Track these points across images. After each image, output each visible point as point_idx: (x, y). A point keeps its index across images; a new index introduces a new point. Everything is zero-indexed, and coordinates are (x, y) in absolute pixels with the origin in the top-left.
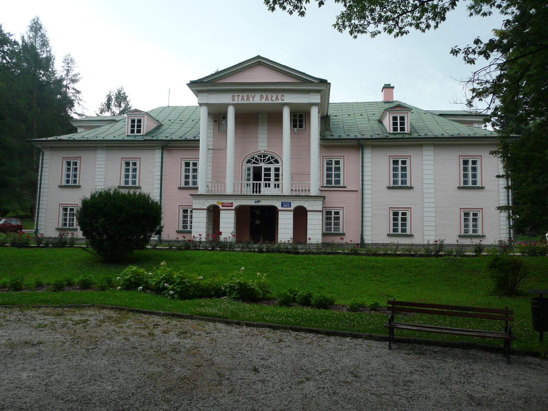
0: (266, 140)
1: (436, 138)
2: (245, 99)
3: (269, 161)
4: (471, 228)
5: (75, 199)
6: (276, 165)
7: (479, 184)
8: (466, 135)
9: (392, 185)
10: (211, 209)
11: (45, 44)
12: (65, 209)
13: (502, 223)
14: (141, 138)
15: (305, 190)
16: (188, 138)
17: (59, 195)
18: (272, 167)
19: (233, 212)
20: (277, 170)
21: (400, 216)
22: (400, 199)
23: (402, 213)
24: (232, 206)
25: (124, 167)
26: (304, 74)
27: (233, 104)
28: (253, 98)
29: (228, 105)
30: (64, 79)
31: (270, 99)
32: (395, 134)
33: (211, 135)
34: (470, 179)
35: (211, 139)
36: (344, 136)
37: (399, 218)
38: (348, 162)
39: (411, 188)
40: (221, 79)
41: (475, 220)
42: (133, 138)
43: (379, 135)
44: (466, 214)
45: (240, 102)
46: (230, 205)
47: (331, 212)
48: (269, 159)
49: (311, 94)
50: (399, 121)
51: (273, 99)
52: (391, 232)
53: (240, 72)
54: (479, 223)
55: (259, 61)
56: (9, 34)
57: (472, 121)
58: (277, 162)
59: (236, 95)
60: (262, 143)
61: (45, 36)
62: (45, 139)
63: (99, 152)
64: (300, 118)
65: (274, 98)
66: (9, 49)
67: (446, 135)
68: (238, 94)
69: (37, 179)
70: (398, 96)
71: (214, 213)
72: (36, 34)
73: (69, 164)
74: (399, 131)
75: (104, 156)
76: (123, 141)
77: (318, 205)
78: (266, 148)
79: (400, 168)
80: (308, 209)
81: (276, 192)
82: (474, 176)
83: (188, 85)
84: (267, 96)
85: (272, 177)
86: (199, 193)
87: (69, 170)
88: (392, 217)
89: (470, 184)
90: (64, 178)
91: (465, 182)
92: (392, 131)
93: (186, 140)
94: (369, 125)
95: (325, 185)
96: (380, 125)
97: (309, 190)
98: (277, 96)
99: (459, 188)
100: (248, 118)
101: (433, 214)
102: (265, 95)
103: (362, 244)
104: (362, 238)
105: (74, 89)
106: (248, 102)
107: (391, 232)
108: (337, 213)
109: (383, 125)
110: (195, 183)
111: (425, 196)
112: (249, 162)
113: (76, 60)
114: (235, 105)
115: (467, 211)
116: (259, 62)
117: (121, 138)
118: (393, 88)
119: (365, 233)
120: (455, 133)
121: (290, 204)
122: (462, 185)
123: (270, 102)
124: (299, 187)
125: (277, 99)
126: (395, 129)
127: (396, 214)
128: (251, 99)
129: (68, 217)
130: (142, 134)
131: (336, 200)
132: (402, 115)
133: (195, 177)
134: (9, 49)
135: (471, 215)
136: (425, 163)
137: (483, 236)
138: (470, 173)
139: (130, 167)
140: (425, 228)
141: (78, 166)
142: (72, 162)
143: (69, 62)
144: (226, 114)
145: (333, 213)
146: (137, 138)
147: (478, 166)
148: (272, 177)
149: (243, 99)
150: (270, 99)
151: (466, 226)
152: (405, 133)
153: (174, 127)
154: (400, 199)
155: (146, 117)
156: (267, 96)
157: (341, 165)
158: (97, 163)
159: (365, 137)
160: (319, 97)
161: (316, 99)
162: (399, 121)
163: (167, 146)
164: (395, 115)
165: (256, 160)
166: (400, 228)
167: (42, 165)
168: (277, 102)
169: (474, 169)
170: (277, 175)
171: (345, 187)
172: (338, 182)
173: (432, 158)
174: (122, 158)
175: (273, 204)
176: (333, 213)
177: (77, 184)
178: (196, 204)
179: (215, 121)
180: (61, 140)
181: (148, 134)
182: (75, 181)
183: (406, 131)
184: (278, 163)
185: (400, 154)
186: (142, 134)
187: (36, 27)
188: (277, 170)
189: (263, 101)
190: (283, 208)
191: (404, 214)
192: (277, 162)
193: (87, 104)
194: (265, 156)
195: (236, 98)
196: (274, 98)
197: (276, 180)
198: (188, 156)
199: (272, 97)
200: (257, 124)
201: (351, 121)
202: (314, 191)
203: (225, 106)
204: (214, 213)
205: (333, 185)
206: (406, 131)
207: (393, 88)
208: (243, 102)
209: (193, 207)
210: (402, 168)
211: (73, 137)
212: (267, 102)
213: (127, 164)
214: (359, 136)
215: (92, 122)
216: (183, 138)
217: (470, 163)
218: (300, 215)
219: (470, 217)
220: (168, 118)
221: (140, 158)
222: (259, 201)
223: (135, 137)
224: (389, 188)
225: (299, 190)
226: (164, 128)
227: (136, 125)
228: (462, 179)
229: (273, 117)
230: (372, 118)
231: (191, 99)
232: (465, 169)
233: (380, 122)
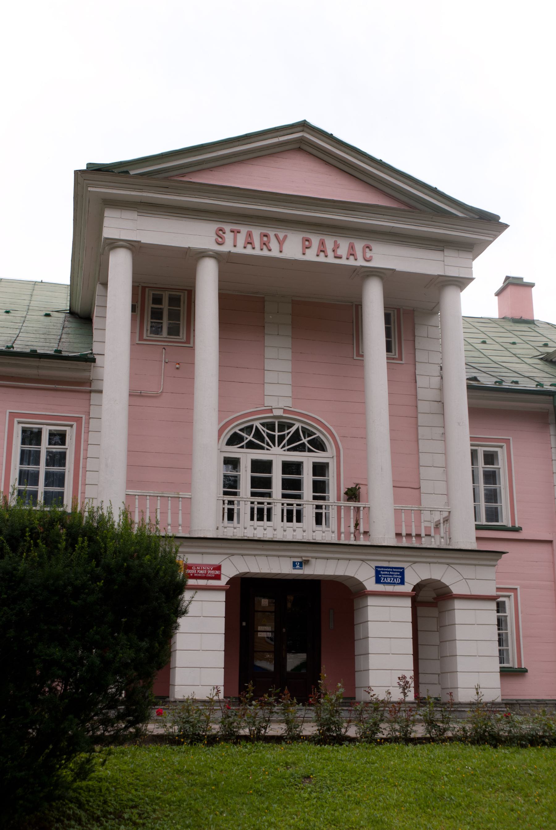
0: (287, 378)
3: (295, 442)
6: (319, 457)
18: (308, 460)
19: (221, 596)
20: (320, 469)
24: (218, 577)
28: (281, 243)
29: (202, 254)
45: (239, 249)
46: (213, 573)
48: (296, 437)
51: (339, 252)
55: (302, 140)
59: (227, 228)
64: (414, 311)
68: (236, 227)
78: (287, 403)
84: (322, 243)
98: (352, 247)
102: (315, 240)
106: (265, 253)
112: (235, 440)
114: (225, 260)
116: (303, 141)
118: (531, 285)
121: (402, 574)
123: (331, 259)
124: (418, 526)
125: (352, 254)
149: (249, 242)
156: (322, 243)
165: (258, 435)
168: (351, 262)
175: (350, 573)
188: (320, 469)
189: (311, 256)
190: (380, 588)
192: (318, 445)
195: (229, 237)
196: (343, 250)
198: (44, 409)
199: (336, 247)
203: (192, 257)
207: (531, 285)
208: (249, 251)
212: (322, 259)
222: (307, 562)
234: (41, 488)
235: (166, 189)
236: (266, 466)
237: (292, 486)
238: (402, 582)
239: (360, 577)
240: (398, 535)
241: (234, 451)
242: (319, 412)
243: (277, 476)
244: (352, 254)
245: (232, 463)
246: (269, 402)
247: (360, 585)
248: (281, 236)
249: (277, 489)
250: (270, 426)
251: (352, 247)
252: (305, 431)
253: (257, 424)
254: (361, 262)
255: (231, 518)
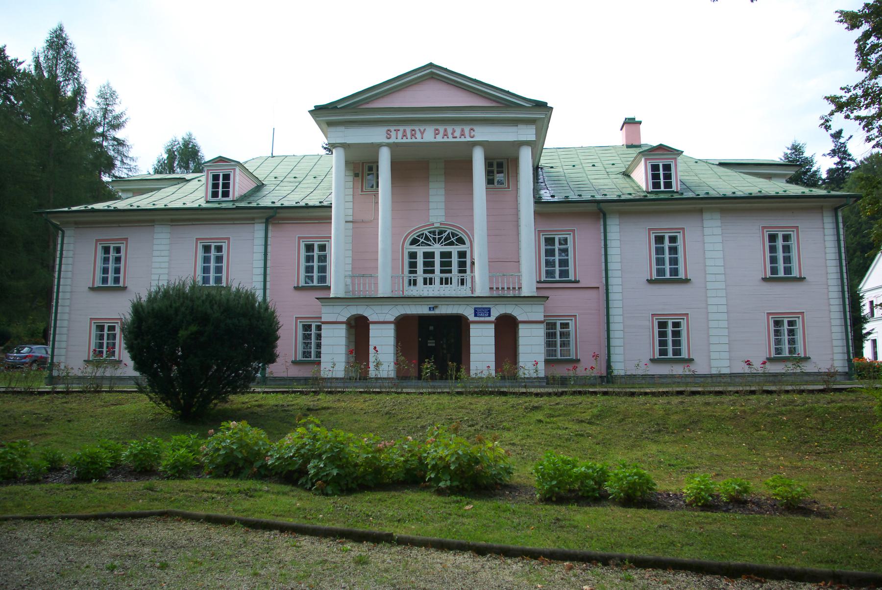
1: (725, 198)
2: (409, 135)
4: (786, 347)
5: (118, 309)
6: (461, 248)
7: (795, 273)
8: (773, 193)
9: (654, 277)
10: (353, 323)
11: (72, 69)
12: (101, 328)
13: (834, 336)
14: (230, 205)
15: (503, 288)
16: (311, 203)
17: (90, 305)
18: (454, 250)
20: (462, 255)
21: (558, 329)
22: (669, 301)
23: (673, 323)
25: (201, 253)
26: (508, 92)
27: (388, 145)
28: (422, 133)
29: (380, 145)
30: (97, 124)
31: (450, 136)
32: (657, 193)
33: (350, 198)
34: (781, 265)
35: (350, 205)
36: (573, 197)
37: (669, 333)
38: (582, 242)
39: (686, 281)
40: (368, 103)
41: (791, 332)
42: (217, 205)
43: (630, 194)
44: (778, 323)
45: (399, 140)
47: (555, 324)
48: (448, 238)
49: (520, 126)
50: (661, 172)
51: (455, 135)
52: (657, 356)
53: (400, 90)
54: (799, 337)
55: (432, 73)
56: (16, 60)
57: (769, 174)
58: (461, 241)
59: (392, 129)
60: (436, 210)
61: (71, 56)
62: (66, 209)
63: (158, 229)
64: (501, 164)
65: (457, 134)
66: (15, 84)
67: (739, 194)
69: (53, 281)
70: (649, 137)
71: (359, 329)
72: (58, 53)
73: (106, 250)
74: (662, 189)
75: (168, 236)
76: (199, 209)
77: (537, 313)
78: (442, 219)
79: (666, 249)
80: (371, 319)
81: (464, 291)
82: (787, 260)
83: (311, 112)
84: (445, 130)
85: (455, 267)
86: (332, 296)
87: (106, 260)
88: (656, 330)
89: (781, 274)
90: (99, 275)
91: (774, 270)
92: (651, 189)
93: (307, 207)
94: (609, 180)
95: (543, 278)
96: (628, 180)
97: (520, 288)
98: (463, 130)
99: (765, 279)
100: (412, 168)
101: (725, 324)
102: (442, 129)
103: (608, 377)
104: (609, 367)
105: (115, 139)
106: (414, 140)
107: (657, 356)
108: (565, 325)
109: (633, 181)
110: (323, 279)
111: (710, 294)
112: (414, 242)
113: (119, 92)
114: (393, 147)
115: (778, 318)
116: (432, 74)
117: (196, 205)
118: (640, 123)
119: (614, 358)
120: (754, 191)
122: (769, 275)
123: (451, 139)
124: (503, 283)
125: (463, 134)
126: (656, 185)
127: (662, 325)
128: (418, 135)
129: (105, 341)
130: (231, 198)
131: (564, 303)
132: (666, 162)
133: (323, 269)
134: (15, 84)
135: (786, 323)
136: (707, 239)
137: (806, 359)
138: (780, 255)
139: (213, 253)
140: (713, 348)
141: (123, 254)
142: (112, 246)
143: (107, 97)
144: (377, 162)
145: (558, 326)
146: (224, 205)
147: (793, 243)
148: (455, 267)
150: (450, 136)
151: (778, 342)
152: (673, 192)
153: (285, 188)
154: (669, 301)
155: (237, 169)
156: (445, 130)
157: (570, 245)
158: (155, 247)
159: (609, 197)
160: (534, 131)
161: (527, 133)
162: (661, 172)
163: (275, 216)
164: (655, 162)
165: (427, 238)
166: (670, 348)
167: (61, 254)
168: (463, 139)
169: (787, 249)
170: (462, 265)
171: (578, 282)
172: (564, 273)
173: (718, 231)
174: (197, 239)
175: (509, 311)
176: (558, 326)
177: (121, 284)
178: (328, 314)
179: (356, 175)
180: (93, 211)
181: (243, 198)
182: (117, 280)
183: (674, 189)
184: (464, 243)
185: (666, 225)
186: (231, 198)
187: (58, 43)
188: (462, 255)
189: (439, 139)
190: (477, 319)
191: (676, 325)
192: (461, 241)
193: (142, 149)
194: (441, 233)
195: (393, 134)
196: (457, 134)
197: (460, 272)
198: (310, 232)
199: (454, 131)
200: (426, 179)
201: (578, 175)
202: (528, 288)
204: (359, 329)
205: (557, 278)
206: (674, 189)
207: (640, 123)
208: (405, 140)
209: (323, 320)
210: (670, 248)
211: (115, 205)
212: (445, 140)
213: (207, 249)
214: (599, 197)
215: (147, 183)
216: (302, 204)
217: (780, 238)
218: (507, 330)
219: (784, 327)
220: (273, 174)
221: (228, 239)
223: (219, 202)
224: (650, 281)
225: (503, 288)
226: (265, 191)
227: (221, 183)
228: (768, 266)
229: (454, 166)
230: (612, 170)
231: (312, 140)
232: (773, 249)
233: (627, 175)
234: (557, 258)
235: (356, 113)
236: (431, 255)
237: (446, 266)
238: (489, 316)
239: (466, 313)
240: (491, 288)
241: (414, 248)
242: (456, 224)
243: (437, 260)
244: (463, 134)
245: (413, 255)
246: (432, 220)
247: (466, 319)
248: (422, 130)
249: (437, 267)
250: (434, 233)
251: (463, 130)
252: (452, 233)
253: (426, 232)
254: (468, 139)
255: (462, 284)
